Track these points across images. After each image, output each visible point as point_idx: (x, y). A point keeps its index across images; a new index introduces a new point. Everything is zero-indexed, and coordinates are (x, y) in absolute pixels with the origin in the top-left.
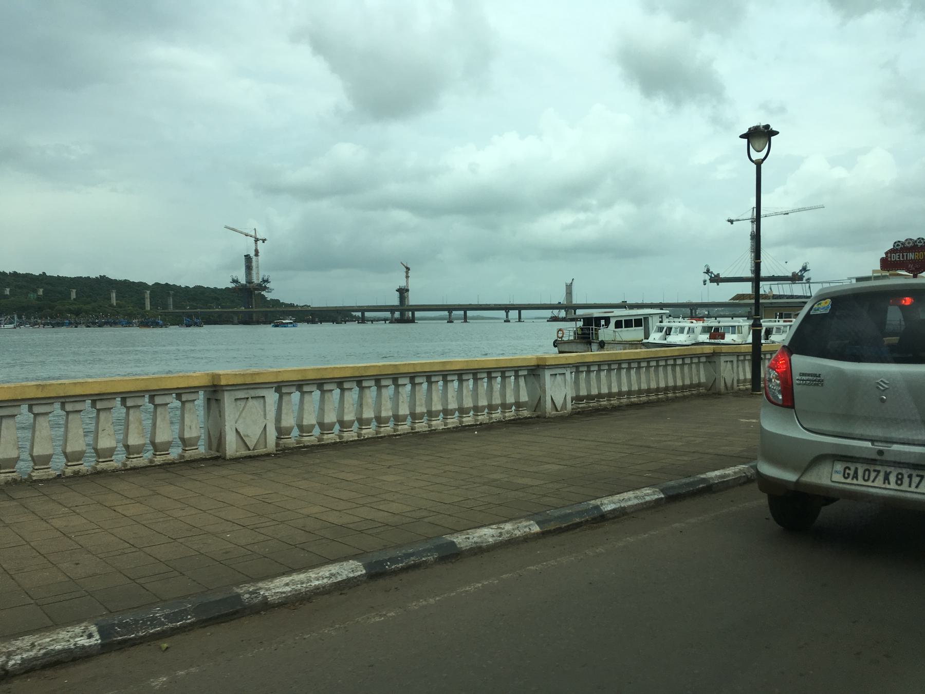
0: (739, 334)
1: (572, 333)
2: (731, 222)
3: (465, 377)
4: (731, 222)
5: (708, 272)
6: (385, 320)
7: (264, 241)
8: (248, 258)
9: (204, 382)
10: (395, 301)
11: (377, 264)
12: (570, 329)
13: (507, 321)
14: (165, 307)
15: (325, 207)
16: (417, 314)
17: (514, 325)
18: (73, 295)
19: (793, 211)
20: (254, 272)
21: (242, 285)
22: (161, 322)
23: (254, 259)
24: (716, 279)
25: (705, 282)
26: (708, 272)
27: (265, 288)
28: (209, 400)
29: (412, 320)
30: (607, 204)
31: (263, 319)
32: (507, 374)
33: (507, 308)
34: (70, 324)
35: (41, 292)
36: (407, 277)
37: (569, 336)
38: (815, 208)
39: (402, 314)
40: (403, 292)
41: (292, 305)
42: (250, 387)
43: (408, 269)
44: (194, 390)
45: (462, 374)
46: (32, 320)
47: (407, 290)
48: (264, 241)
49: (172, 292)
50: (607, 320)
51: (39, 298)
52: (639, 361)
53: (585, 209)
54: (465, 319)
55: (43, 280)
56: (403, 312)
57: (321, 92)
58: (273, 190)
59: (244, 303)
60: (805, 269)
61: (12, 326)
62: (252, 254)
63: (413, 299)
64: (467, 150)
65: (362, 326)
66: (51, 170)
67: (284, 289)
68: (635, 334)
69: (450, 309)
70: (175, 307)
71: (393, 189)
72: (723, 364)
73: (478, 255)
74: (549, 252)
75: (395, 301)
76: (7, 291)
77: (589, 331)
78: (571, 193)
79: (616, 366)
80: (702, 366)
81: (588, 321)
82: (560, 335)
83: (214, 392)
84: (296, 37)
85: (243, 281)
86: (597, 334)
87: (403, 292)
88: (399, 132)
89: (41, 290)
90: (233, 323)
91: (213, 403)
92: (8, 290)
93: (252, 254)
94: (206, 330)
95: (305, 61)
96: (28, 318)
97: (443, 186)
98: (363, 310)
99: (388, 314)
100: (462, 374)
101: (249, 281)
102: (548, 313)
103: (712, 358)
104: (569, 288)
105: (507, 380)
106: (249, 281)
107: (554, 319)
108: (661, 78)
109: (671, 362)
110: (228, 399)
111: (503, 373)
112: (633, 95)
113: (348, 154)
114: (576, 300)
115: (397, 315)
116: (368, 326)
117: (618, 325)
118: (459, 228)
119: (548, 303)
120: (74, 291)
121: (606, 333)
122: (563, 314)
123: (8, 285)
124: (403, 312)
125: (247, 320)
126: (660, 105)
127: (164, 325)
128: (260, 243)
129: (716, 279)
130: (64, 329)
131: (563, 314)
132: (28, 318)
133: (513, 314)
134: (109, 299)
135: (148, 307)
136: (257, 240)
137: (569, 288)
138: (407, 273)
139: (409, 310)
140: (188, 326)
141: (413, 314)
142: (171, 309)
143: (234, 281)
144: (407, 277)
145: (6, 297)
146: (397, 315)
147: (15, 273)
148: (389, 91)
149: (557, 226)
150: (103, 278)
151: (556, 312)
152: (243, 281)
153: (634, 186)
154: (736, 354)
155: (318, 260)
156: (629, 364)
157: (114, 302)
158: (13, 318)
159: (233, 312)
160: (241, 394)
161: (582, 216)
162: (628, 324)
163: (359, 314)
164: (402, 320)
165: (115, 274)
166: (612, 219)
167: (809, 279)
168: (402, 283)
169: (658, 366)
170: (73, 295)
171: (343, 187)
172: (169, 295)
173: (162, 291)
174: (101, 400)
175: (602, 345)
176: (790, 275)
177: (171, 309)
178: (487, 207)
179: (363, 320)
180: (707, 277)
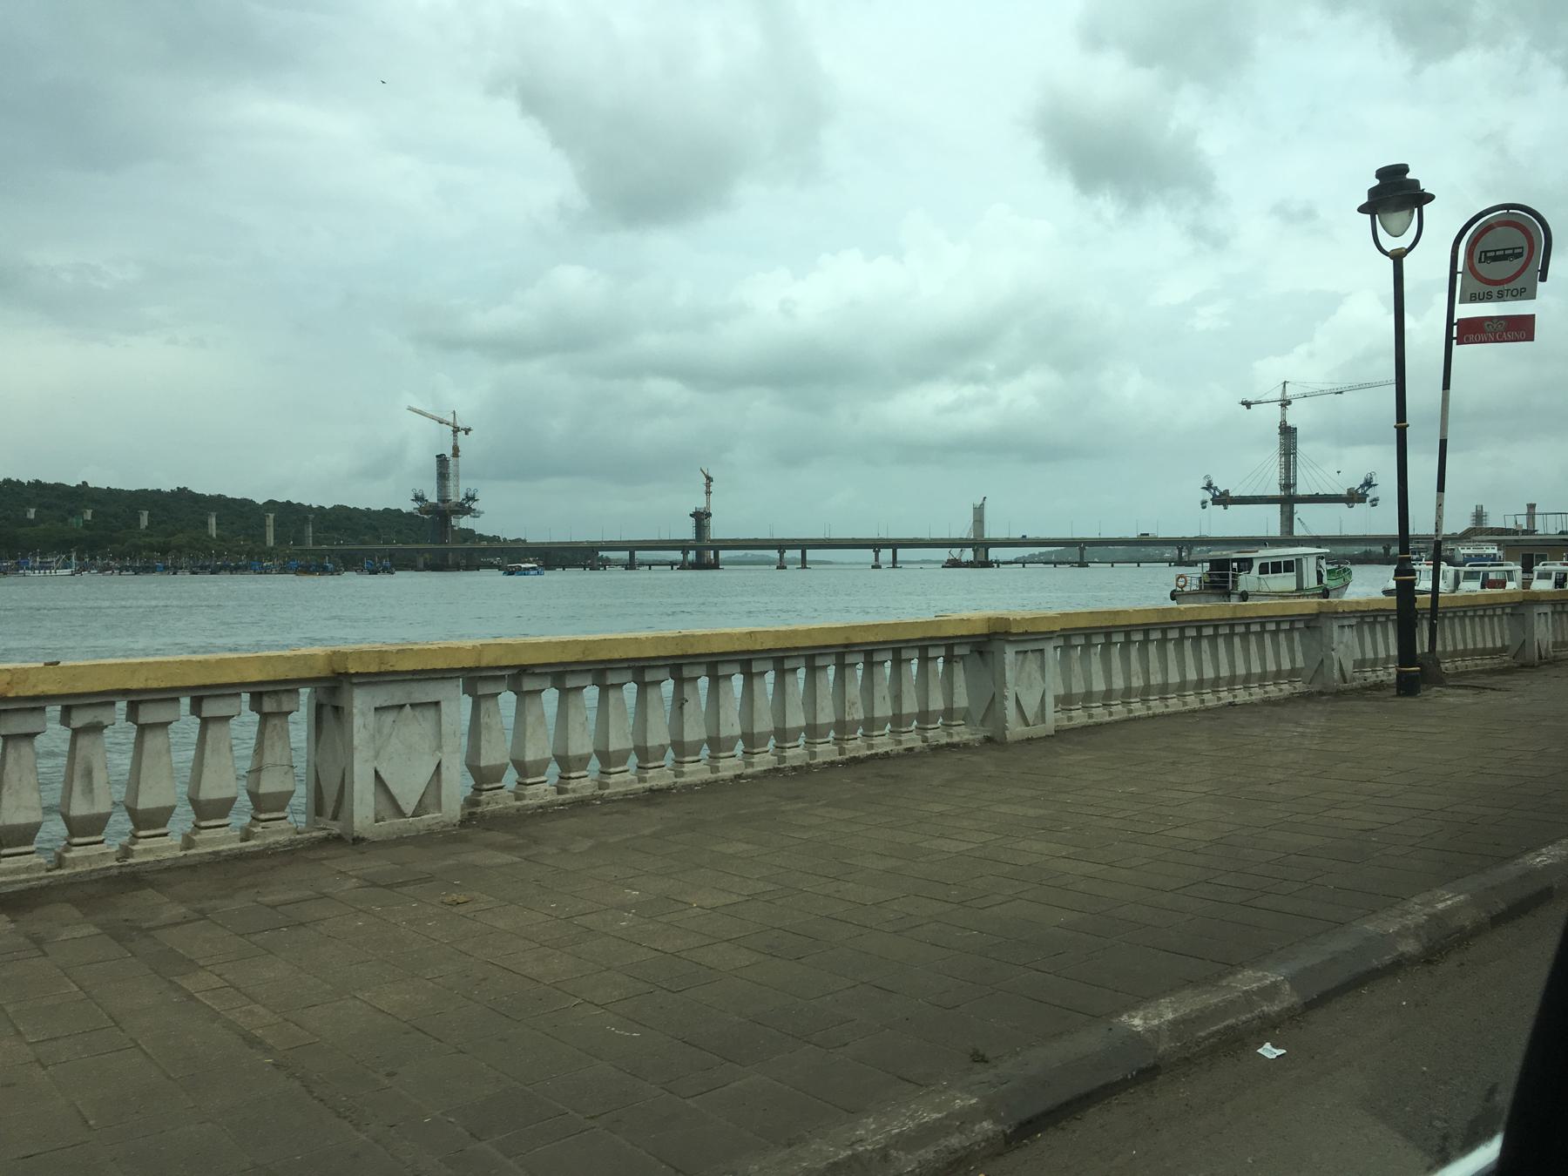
0: (1370, 585)
1: (1196, 582)
2: (1248, 405)
3: (819, 662)
4: (1248, 405)
5: (1209, 487)
6: (672, 564)
7: (467, 431)
8: (442, 459)
9: (321, 670)
10: (687, 532)
11: (629, 469)
12: (1195, 575)
13: (876, 567)
14: (299, 541)
15: (534, 370)
16: (723, 554)
17: (792, 572)
18: (144, 521)
19: (1351, 389)
20: (451, 484)
21: (432, 505)
22: (330, 566)
23: (452, 461)
24: (1223, 499)
25: (1204, 504)
26: (1209, 487)
27: (469, 511)
28: (319, 708)
29: (715, 565)
30: (1012, 371)
31: (244, 561)
32: (932, 653)
33: (876, 545)
34: (166, 568)
35: (88, 515)
36: (708, 493)
37: (1194, 586)
38: (1370, 386)
39: (698, 555)
40: (701, 518)
41: (495, 539)
42: (408, 679)
43: (709, 479)
44: (288, 687)
45: (872, 651)
46: (99, 562)
47: (709, 515)
48: (467, 431)
49: (311, 516)
50: (1250, 561)
51: (87, 525)
52: (1199, 625)
53: (976, 378)
54: (804, 563)
55: (83, 495)
56: (977, 551)
57: (534, 178)
58: (451, 344)
59: (428, 537)
60: (1368, 483)
61: (68, 571)
62: (449, 453)
63: (718, 529)
64: (779, 278)
65: (631, 574)
66: (73, 307)
67: (497, 514)
68: (1285, 582)
69: (782, 545)
70: (317, 542)
71: (652, 342)
72: (1335, 627)
73: (793, 455)
74: (916, 451)
75: (687, 532)
76: (32, 514)
77: (1221, 578)
78: (951, 352)
79: (1080, 641)
80: (1296, 636)
81: (1220, 565)
82: (1181, 583)
83: (333, 687)
84: (495, 88)
85: (433, 498)
86: (1235, 583)
87: (701, 518)
88: (662, 246)
89: (89, 512)
90: (415, 568)
91: (328, 714)
92: (33, 511)
93: (449, 453)
94: (404, 580)
95: (509, 127)
96: (93, 558)
97: (735, 340)
98: (632, 547)
99: (677, 555)
100: (813, 657)
101: (443, 499)
102: (944, 554)
103: (1312, 624)
104: (979, 512)
105: (819, 675)
106: (443, 499)
107: (954, 564)
108: (1109, 160)
109: (1225, 630)
110: (361, 703)
111: (869, 654)
112: (1063, 189)
113: (575, 283)
114: (991, 533)
115: (692, 555)
116: (642, 574)
117: (1264, 569)
118: (762, 409)
119: (946, 536)
120: (146, 513)
121: (1248, 581)
122: (968, 554)
123: (30, 504)
124: (701, 551)
125: (439, 564)
126: (1107, 204)
127: (336, 571)
128: (461, 434)
129: (1223, 499)
130: (155, 577)
131: (968, 554)
132: (93, 558)
133: (886, 554)
134: (205, 524)
135: (271, 542)
136: (456, 430)
137: (979, 512)
138: (708, 486)
139: (710, 548)
140: (374, 572)
141: (716, 555)
142: (310, 545)
143: (418, 498)
144: (708, 493)
145: (31, 523)
146: (692, 555)
147: (38, 482)
148: (651, 177)
149: (926, 406)
150: (182, 492)
151: (956, 552)
152: (433, 498)
153: (1058, 339)
154: (1366, 617)
155: (527, 464)
156: (1127, 634)
157: (213, 530)
158: (69, 558)
159: (418, 550)
160: (396, 694)
161: (969, 391)
162: (1276, 568)
163: (625, 555)
164: (699, 565)
165: (205, 485)
166: (1020, 396)
167: (1376, 500)
168: (700, 503)
169: (1182, 638)
170: (144, 521)
171: (568, 339)
172: (306, 518)
173: (290, 515)
174: (573, 672)
175: (1244, 596)
176: (1344, 492)
177: (310, 545)
178: (808, 373)
179: (631, 565)
180: (1208, 496)
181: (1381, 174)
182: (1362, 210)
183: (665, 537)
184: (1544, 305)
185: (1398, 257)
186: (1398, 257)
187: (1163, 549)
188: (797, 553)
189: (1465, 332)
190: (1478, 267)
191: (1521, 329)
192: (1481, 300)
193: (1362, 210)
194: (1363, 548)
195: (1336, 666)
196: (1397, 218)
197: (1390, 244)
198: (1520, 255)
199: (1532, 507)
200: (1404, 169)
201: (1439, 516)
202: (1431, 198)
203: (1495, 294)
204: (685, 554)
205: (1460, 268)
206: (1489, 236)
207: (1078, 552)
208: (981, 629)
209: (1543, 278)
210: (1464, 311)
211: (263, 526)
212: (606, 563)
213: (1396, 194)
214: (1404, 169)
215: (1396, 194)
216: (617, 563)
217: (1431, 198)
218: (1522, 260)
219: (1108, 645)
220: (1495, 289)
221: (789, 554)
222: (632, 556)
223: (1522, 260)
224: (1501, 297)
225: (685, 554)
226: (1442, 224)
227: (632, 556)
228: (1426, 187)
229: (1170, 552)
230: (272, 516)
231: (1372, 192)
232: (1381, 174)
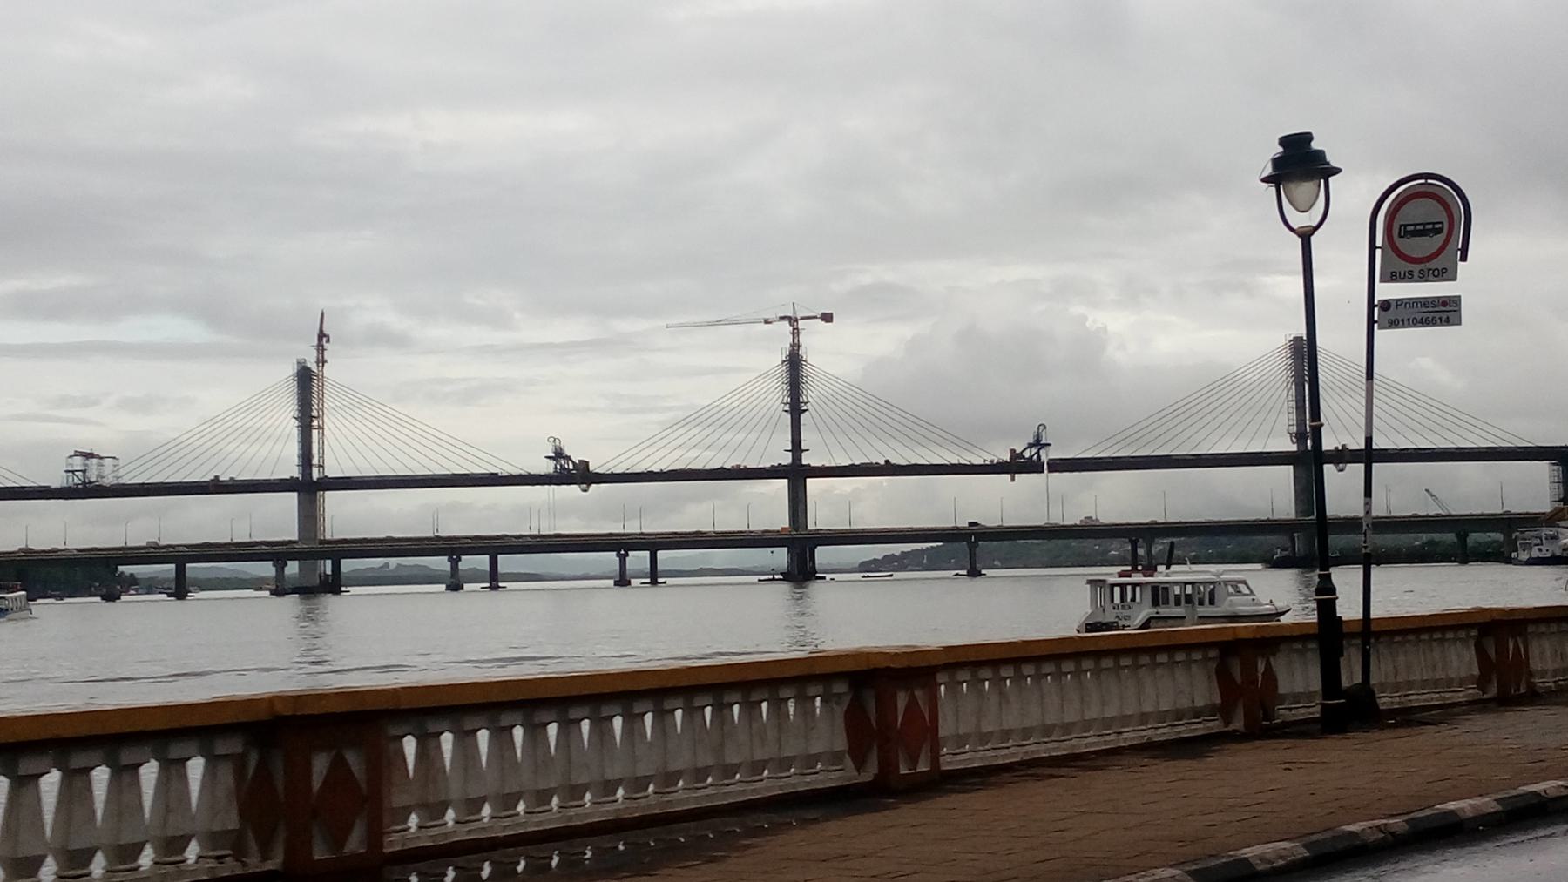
13: (623, 581)
16: (348, 565)
139: (324, 556)
141: (336, 567)
146: (292, 568)
181: (1285, 141)
183: (242, 537)
184: (1468, 283)
185: (1306, 236)
186: (1306, 236)
187: (1107, 542)
188: (482, 562)
189: (1382, 315)
190: (1399, 242)
191: (1444, 312)
192: (1402, 280)
194: (1425, 537)
195: (393, 320)
196: (1304, 189)
197: (1298, 220)
198: (1440, 231)
199: (654, 582)
200: (1306, 138)
201: (1368, 504)
202: (1337, 171)
203: (1416, 274)
204: (280, 569)
205: (1379, 243)
206: (1406, 208)
207: (970, 548)
209: (1464, 258)
210: (1385, 291)
212: (132, 584)
213: (1299, 164)
214: (1306, 138)
215: (1299, 164)
216: (150, 586)
217: (1337, 171)
218: (1441, 238)
220: (1416, 268)
221: (468, 562)
222: (181, 572)
223: (1441, 238)
224: (1423, 277)
225: (280, 569)
226: (1355, 196)
227: (181, 572)
228: (1333, 160)
229: (1119, 547)
231: (1276, 162)
232: (1285, 141)
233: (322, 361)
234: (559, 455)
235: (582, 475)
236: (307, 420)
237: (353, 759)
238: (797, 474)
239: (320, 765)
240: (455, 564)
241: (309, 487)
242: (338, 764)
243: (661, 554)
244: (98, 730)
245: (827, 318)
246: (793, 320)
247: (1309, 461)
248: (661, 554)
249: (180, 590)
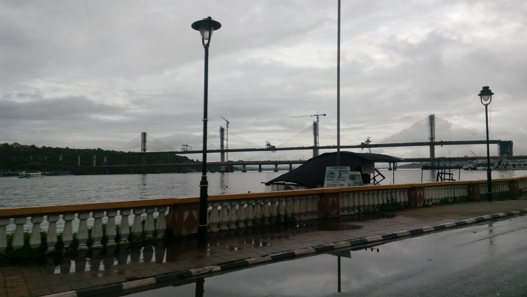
43: (228, 122)
138: (227, 124)
179: (260, 170)
181: (484, 88)
182: (479, 95)
185: (486, 105)
186: (486, 105)
193: (479, 95)
196: (486, 97)
197: (485, 103)
200: (488, 87)
202: (493, 94)
208: (411, 187)
211: (93, 160)
214: (488, 87)
216: (237, 169)
217: (493, 94)
219: (383, 193)
222: (260, 166)
227: (260, 166)
228: (492, 92)
230: (95, 156)
231: (482, 91)
233: (318, 121)
234: (268, 145)
235: (272, 149)
236: (316, 134)
237: (335, 199)
238: (432, 144)
239: (186, 215)
240: (276, 166)
241: (338, 147)
242: (420, 193)
243: (262, 166)
244: (277, 195)
245: (325, 115)
246: (317, 116)
247: (205, 151)
248: (262, 166)
249: (244, 171)
